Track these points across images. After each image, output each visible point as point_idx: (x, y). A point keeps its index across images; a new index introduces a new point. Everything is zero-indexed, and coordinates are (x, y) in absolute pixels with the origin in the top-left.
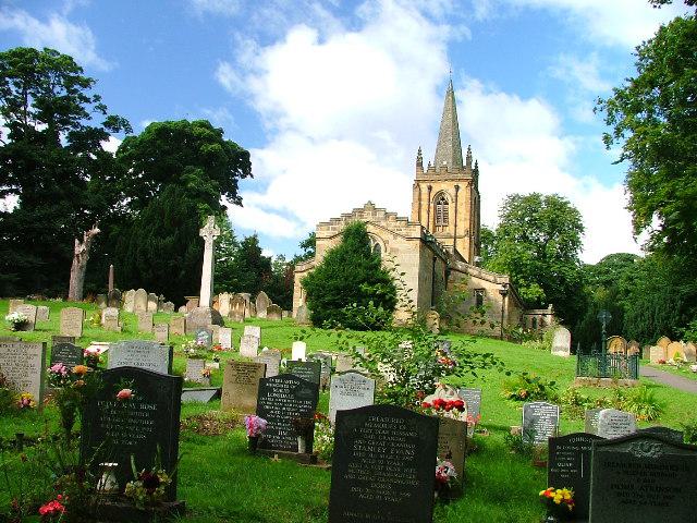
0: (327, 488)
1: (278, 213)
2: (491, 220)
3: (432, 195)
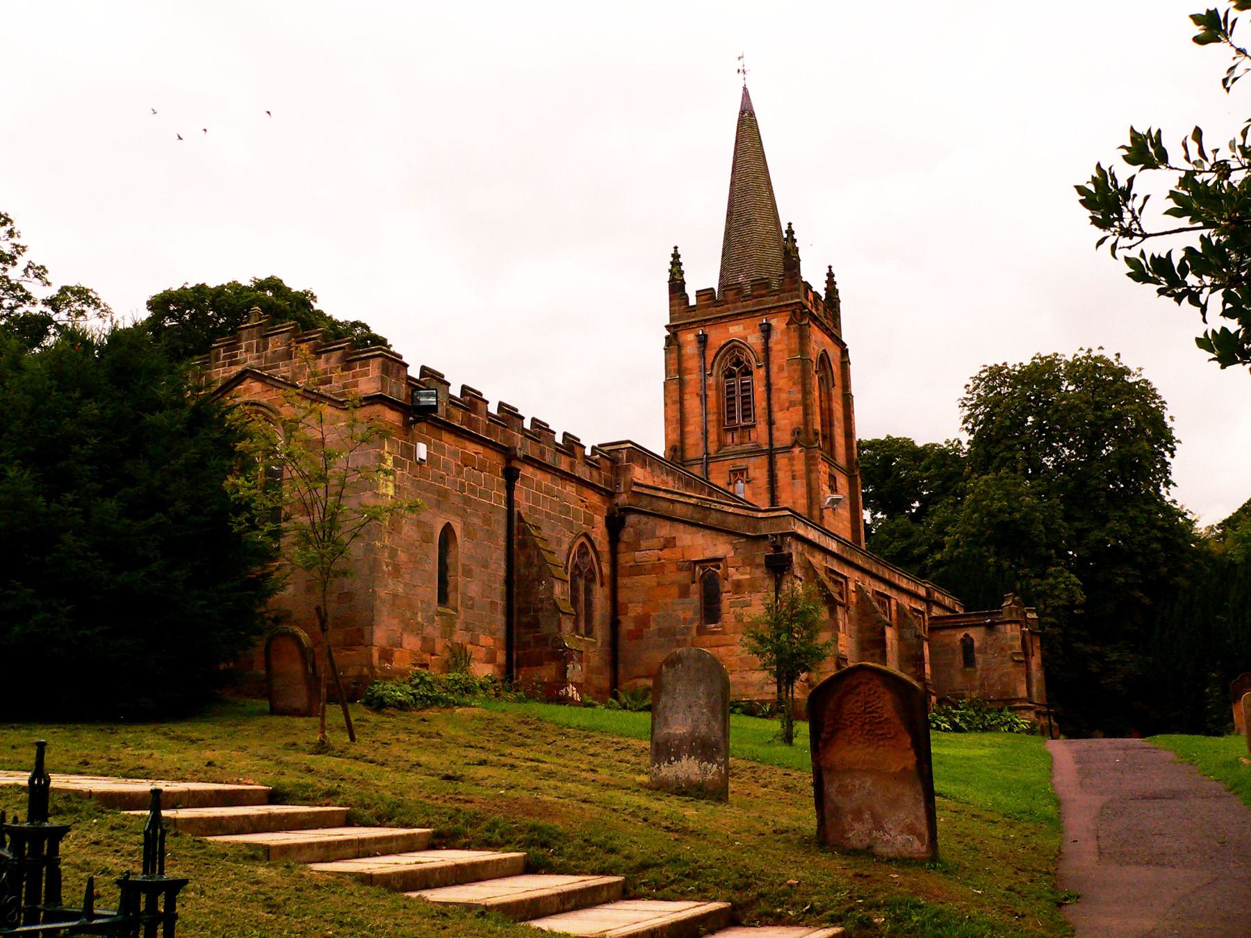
0: (63, 890)
3: (710, 354)
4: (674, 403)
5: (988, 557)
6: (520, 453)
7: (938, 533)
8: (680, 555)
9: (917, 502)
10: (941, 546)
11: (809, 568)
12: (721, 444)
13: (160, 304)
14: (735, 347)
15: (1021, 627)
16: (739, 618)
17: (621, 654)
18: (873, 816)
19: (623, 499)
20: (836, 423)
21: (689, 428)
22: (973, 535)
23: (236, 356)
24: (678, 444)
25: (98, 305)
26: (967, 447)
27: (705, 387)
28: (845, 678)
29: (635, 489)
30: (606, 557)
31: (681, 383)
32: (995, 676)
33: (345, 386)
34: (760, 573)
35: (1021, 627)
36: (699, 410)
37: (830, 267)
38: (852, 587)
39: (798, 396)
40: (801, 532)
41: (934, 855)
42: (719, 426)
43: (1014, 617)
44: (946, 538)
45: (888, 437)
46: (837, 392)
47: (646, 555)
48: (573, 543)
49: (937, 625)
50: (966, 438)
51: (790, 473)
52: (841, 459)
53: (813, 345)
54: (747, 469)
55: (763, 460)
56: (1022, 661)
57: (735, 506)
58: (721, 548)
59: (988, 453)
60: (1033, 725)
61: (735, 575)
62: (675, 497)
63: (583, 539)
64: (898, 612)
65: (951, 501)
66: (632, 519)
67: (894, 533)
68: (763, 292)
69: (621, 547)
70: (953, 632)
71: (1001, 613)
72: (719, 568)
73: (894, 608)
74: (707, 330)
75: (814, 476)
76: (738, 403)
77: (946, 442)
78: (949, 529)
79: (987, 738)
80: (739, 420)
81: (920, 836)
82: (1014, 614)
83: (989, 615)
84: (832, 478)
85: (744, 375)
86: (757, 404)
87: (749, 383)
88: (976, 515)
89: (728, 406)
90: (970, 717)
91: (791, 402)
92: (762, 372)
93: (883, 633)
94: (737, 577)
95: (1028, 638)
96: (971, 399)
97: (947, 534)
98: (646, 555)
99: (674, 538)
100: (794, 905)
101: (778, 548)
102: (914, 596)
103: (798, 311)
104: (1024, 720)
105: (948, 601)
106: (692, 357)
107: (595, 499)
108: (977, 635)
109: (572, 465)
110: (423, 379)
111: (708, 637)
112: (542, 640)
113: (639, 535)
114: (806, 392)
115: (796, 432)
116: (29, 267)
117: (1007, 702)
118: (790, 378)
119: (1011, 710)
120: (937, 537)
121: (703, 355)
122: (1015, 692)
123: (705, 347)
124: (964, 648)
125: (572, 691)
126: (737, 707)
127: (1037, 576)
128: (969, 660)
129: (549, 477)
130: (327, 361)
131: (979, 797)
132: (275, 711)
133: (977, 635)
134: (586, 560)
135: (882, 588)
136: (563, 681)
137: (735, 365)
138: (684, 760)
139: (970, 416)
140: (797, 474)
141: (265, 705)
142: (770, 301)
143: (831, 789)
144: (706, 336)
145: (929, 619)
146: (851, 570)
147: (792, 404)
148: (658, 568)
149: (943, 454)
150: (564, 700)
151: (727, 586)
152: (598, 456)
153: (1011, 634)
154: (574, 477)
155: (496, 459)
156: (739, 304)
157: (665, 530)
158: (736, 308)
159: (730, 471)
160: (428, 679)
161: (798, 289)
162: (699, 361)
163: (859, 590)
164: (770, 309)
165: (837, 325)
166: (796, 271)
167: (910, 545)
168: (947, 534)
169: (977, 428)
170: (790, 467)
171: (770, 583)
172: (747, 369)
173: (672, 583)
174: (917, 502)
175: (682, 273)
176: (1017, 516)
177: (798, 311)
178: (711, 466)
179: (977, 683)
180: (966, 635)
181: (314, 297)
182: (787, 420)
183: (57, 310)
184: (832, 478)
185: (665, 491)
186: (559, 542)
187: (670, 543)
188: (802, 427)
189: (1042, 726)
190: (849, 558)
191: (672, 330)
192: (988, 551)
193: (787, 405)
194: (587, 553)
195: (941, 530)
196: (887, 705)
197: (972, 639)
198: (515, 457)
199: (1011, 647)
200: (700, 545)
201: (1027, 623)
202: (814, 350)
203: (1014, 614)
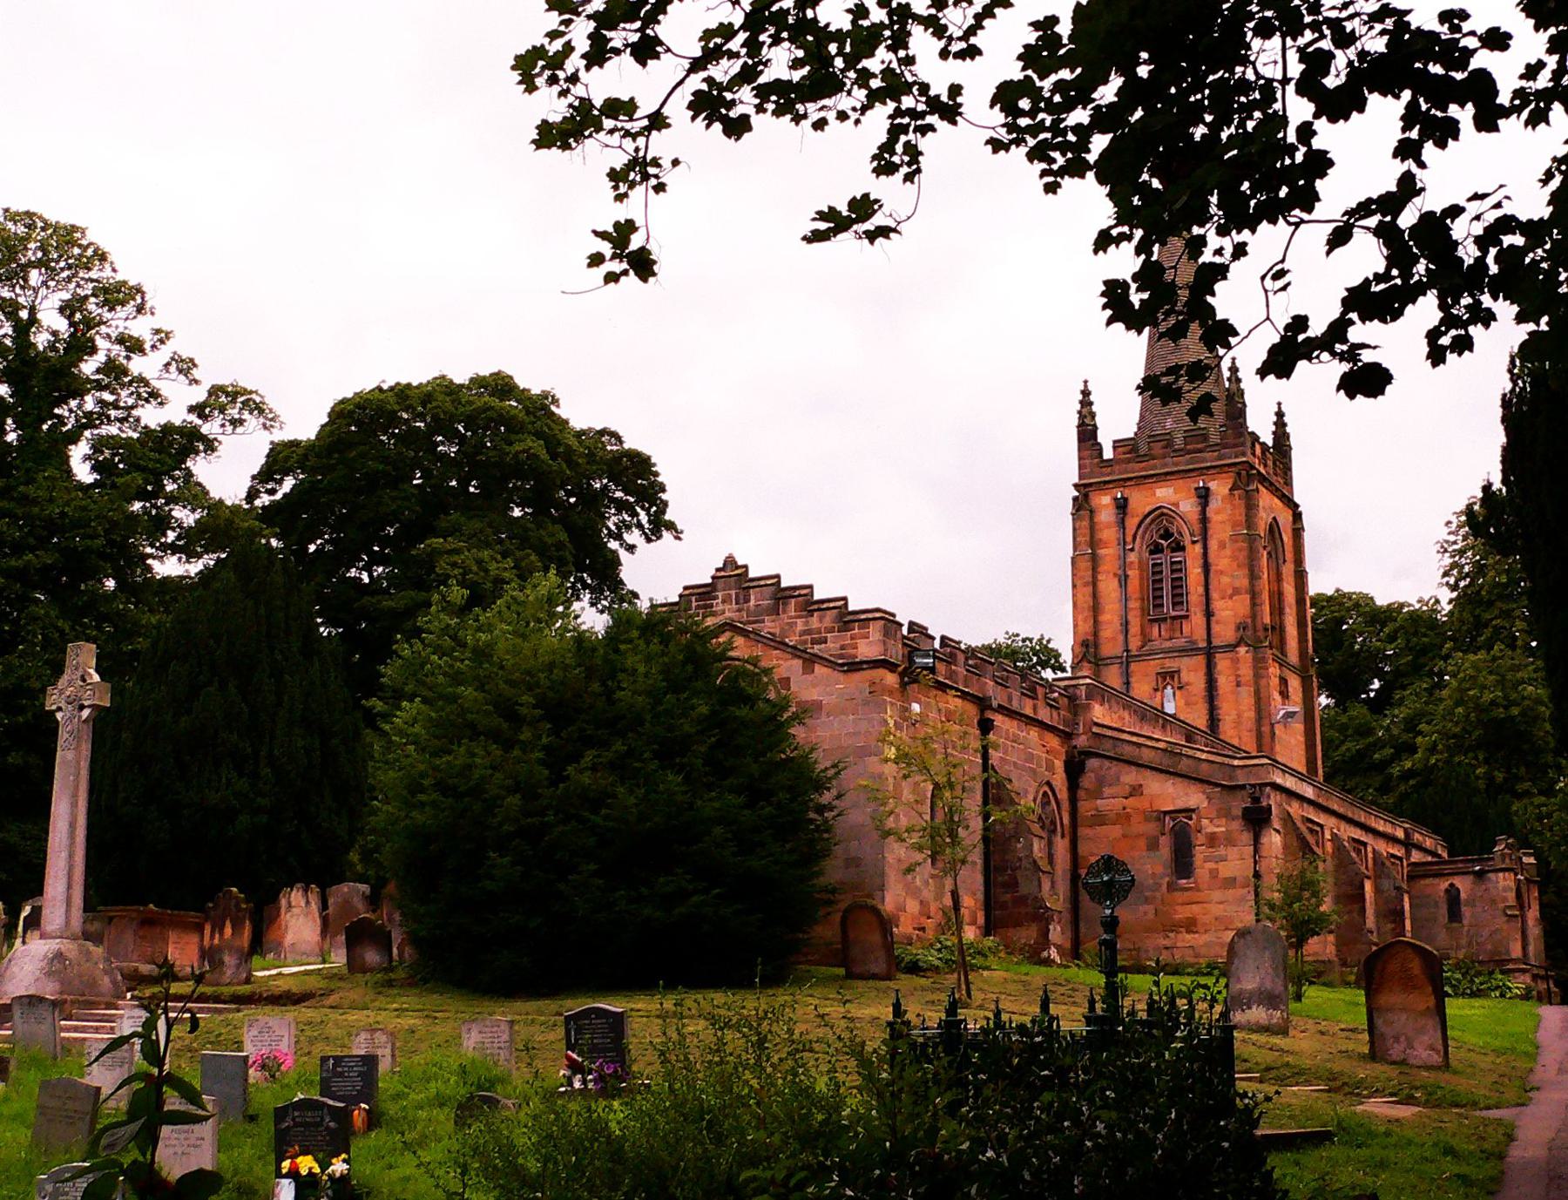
1: (1095, 596)
2: (150, 561)
3: (1132, 523)
4: (1085, 585)
5: (1475, 767)
6: (995, 704)
7: (1407, 730)
8: (1147, 805)
9: (1376, 681)
10: (1413, 749)
11: (1288, 819)
12: (1146, 639)
13: (343, 413)
14: (1163, 514)
15: (1516, 874)
16: (1214, 874)
17: (1081, 913)
18: (1407, 1039)
19: (1082, 741)
20: (1287, 610)
21: (1104, 618)
22: (1455, 736)
23: (712, 606)
24: (1091, 638)
25: (261, 411)
26: (1448, 608)
27: (1125, 566)
28: (1386, 951)
29: (1095, 729)
30: (1065, 805)
31: (1095, 560)
32: (1486, 933)
33: (842, 648)
34: (1236, 825)
35: (1516, 874)
36: (1118, 594)
37: (1279, 404)
38: (1328, 836)
39: (1244, 582)
40: (1279, 781)
41: (1446, 1065)
42: (1143, 615)
43: (1507, 863)
44: (1419, 739)
45: (1338, 590)
46: (1288, 569)
47: (1109, 803)
48: (1037, 792)
49: (1418, 873)
50: (1446, 596)
51: (1232, 678)
52: (1293, 657)
53: (1262, 514)
54: (1178, 672)
55: (1200, 660)
56: (1516, 916)
57: (1208, 752)
58: (1194, 797)
59: (1477, 617)
60: (1528, 990)
61: (1208, 827)
62: (1141, 740)
63: (1046, 788)
64: (1374, 859)
65: (1425, 686)
66: (1092, 763)
67: (1347, 730)
68: (1199, 446)
69: (1081, 794)
70: (1436, 881)
71: (1493, 859)
72: (1191, 819)
73: (1370, 855)
74: (1127, 493)
75: (1263, 682)
76: (1167, 587)
77: (1419, 601)
78: (1423, 727)
79: (1477, 1002)
80: (1168, 609)
81: (1438, 1052)
82: (1507, 861)
83: (1479, 861)
84: (1284, 682)
85: (1173, 550)
86: (1192, 589)
87: (1180, 562)
88: (1460, 710)
89: (1154, 590)
90: (1457, 980)
91: (1234, 589)
92: (1198, 548)
93: (1363, 887)
94: (1211, 829)
95: (1524, 889)
96: (1455, 543)
97: (1420, 733)
98: (1109, 803)
99: (1141, 786)
100: (1366, 1088)
101: (1256, 800)
102: (1392, 839)
103: (1244, 473)
104: (1518, 984)
105: (1428, 843)
106: (1108, 526)
107: (1054, 742)
108: (1463, 884)
109: (1035, 708)
110: (912, 635)
111: (1180, 893)
112: (1022, 901)
113: (1101, 782)
114: (1253, 576)
115: (1241, 627)
116: (173, 359)
117: (1500, 963)
118: (1234, 558)
119: (1503, 972)
120: (1405, 737)
121: (1122, 524)
122: (1508, 952)
123: (1125, 514)
124: (1448, 900)
125: (1053, 953)
126: (1215, 968)
127: (1541, 793)
128: (1454, 913)
129: (1015, 723)
130: (821, 620)
131: (1472, 1039)
132: (850, 975)
133: (1463, 884)
134: (1048, 809)
135: (1357, 834)
136: (1044, 943)
137: (1162, 537)
138: (1254, 1007)
139: (1454, 565)
140: (1242, 680)
141: (841, 971)
142: (1209, 459)
143: (1379, 1022)
144: (1126, 500)
145: (1408, 865)
146: (1327, 816)
147: (1236, 591)
148: (1124, 818)
149: (1415, 617)
150: (1048, 962)
151: (1201, 839)
152: (1056, 695)
153: (1504, 883)
154: (1037, 721)
155: (972, 710)
156: (1169, 460)
157: (1130, 777)
158: (1166, 465)
159: (1158, 674)
160: (949, 943)
161: (1243, 444)
162: (1118, 531)
163: (1335, 837)
164: (1208, 468)
165: (1288, 482)
166: (1241, 420)
167: (1370, 745)
168: (1420, 733)
169: (1462, 584)
170: (1233, 670)
171: (1247, 837)
172: (1178, 544)
173: (1138, 836)
174: (1376, 681)
175: (1093, 415)
176: (1515, 711)
177: (1244, 473)
178: (1133, 666)
179: (1464, 942)
180: (1452, 885)
181: (555, 401)
182: (1229, 612)
183: (204, 417)
184: (1284, 682)
185: (1129, 733)
186: (1026, 792)
187: (1136, 791)
188: (1249, 621)
189: (1539, 992)
190: (1325, 804)
191: (1083, 491)
192: (1476, 758)
193: (1230, 592)
194: (1049, 803)
195: (1411, 725)
196: (1416, 966)
197: (1458, 890)
198: (990, 707)
199: (1505, 899)
200: (1170, 794)
201: (1522, 869)
202: (1263, 519)
203: (1507, 861)
